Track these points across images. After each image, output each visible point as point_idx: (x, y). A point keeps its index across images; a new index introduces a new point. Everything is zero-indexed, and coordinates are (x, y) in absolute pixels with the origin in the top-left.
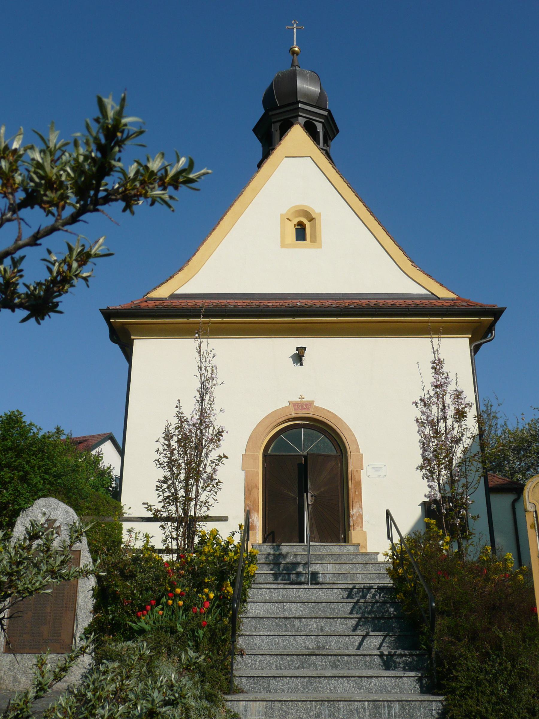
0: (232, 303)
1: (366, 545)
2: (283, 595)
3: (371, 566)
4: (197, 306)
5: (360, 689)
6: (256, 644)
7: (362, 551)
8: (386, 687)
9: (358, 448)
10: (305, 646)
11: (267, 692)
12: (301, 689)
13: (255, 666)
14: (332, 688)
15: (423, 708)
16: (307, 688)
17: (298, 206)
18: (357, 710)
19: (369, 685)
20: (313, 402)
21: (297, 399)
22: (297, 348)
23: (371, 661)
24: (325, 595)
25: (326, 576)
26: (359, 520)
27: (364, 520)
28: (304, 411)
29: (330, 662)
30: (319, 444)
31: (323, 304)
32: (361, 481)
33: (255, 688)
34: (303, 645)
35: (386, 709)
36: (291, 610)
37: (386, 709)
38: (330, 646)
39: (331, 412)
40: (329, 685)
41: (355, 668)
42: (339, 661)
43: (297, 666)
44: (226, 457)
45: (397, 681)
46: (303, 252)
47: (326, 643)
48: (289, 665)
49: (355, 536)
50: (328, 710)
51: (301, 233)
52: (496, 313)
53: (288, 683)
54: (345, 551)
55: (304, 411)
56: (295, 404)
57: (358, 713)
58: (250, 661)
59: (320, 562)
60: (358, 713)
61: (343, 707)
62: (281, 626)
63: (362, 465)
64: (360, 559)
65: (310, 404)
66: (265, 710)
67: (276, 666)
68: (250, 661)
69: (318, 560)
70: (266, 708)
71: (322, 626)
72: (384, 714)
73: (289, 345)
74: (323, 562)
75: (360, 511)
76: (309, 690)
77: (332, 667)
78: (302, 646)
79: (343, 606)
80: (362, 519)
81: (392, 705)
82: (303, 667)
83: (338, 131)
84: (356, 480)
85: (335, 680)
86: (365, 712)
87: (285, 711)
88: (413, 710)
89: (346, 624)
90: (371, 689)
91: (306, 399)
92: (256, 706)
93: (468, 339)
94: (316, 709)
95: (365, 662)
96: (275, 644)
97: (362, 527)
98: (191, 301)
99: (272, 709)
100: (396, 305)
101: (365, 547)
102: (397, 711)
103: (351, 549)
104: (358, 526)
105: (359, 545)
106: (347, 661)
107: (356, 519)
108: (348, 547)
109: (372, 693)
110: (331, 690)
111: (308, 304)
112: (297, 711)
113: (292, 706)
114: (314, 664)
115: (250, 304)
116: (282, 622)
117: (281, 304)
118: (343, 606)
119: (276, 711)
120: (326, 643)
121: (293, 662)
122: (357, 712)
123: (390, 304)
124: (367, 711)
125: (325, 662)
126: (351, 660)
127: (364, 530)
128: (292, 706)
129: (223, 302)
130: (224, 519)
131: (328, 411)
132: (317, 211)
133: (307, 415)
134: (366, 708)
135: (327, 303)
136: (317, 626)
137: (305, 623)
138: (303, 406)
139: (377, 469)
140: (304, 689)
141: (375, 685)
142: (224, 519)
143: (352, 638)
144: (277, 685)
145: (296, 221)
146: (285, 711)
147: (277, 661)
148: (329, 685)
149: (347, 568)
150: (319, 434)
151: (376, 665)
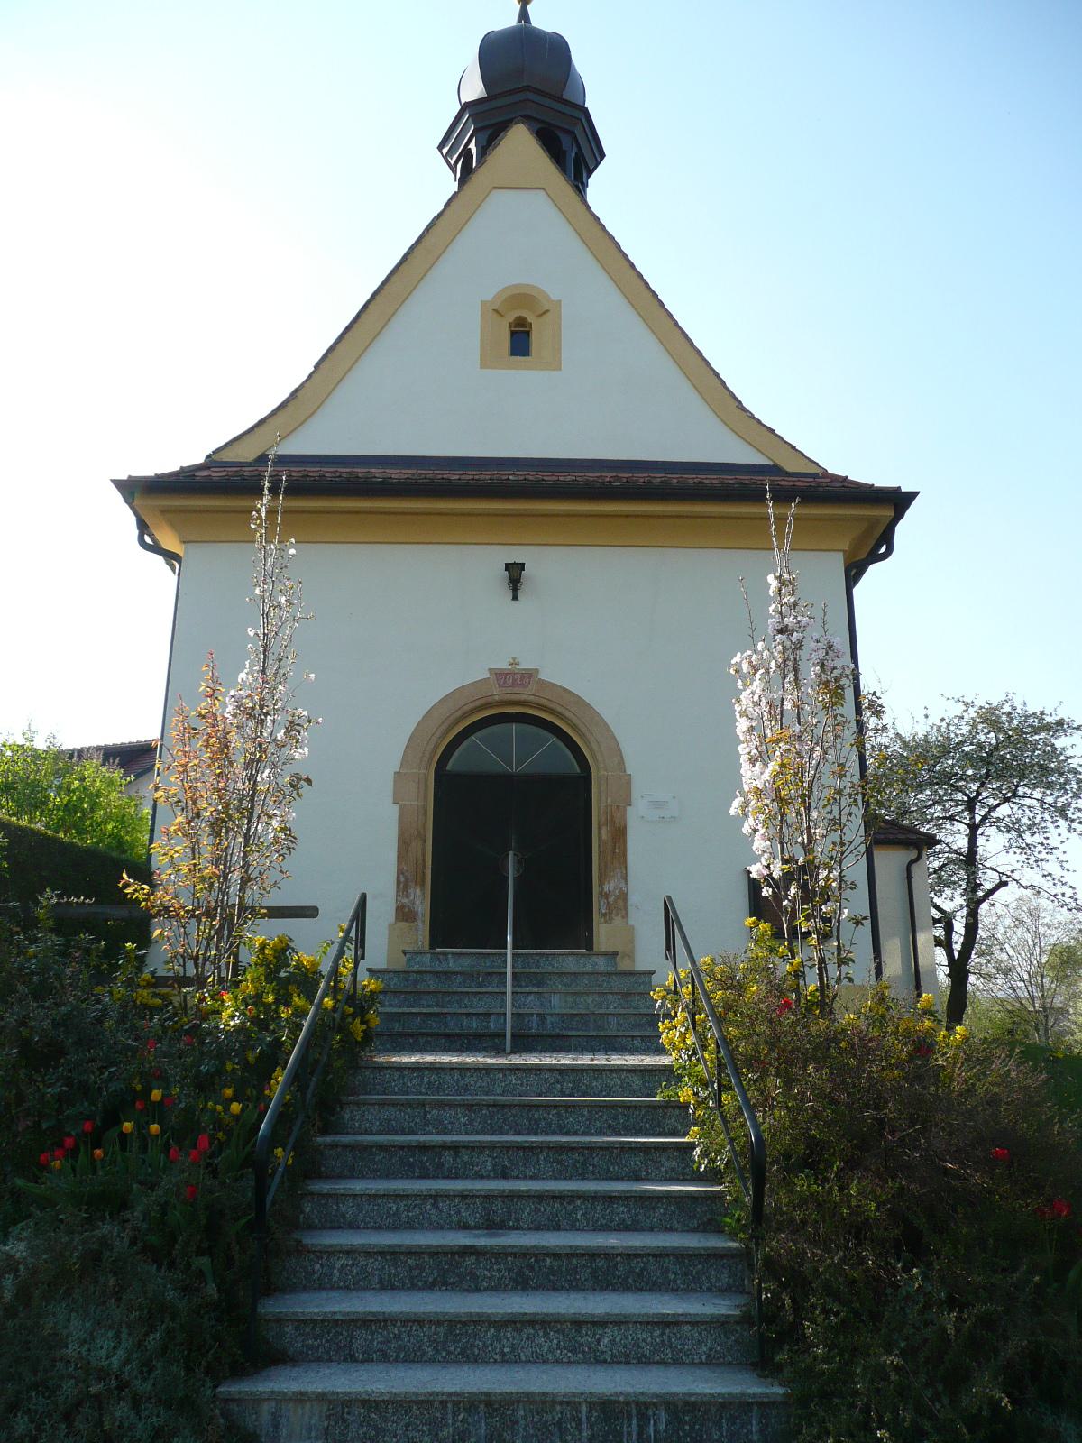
0: (377, 473)
1: (632, 951)
2: (429, 1083)
3: (637, 998)
4: (308, 479)
5: (575, 1352)
6: (344, 1216)
7: (624, 965)
8: (639, 1347)
9: (621, 761)
10: (459, 1222)
11: (345, 1360)
12: (430, 1352)
13: (330, 1280)
14: (506, 1350)
15: (727, 1420)
16: (444, 1349)
17: (516, 286)
18: (559, 1423)
19: (599, 1341)
20: (537, 670)
21: (504, 666)
22: (507, 565)
23: (609, 1267)
24: (522, 1085)
25: (545, 1019)
26: (620, 902)
27: (629, 902)
28: (516, 690)
29: (510, 1270)
30: (539, 756)
31: (561, 478)
32: (625, 827)
33: (317, 1348)
34: (455, 1218)
35: (634, 1422)
36: (441, 1123)
37: (634, 1422)
38: (518, 1220)
39: (570, 692)
40: (499, 1340)
41: (571, 1286)
42: (531, 1268)
43: (430, 1279)
44: (309, 781)
45: (667, 1331)
46: (522, 379)
47: (509, 1213)
48: (412, 1278)
49: (604, 934)
50: (487, 1424)
51: (520, 340)
52: (899, 501)
53: (398, 1337)
54: (589, 968)
55: (516, 690)
56: (499, 675)
57: (563, 1431)
58: (317, 1267)
59: (536, 990)
60: (563, 1431)
61: (525, 1418)
62: (411, 1166)
63: (629, 795)
64: (618, 984)
65: (529, 675)
66: (326, 1424)
67: (381, 1282)
68: (317, 1267)
69: (534, 985)
70: (328, 1418)
71: (504, 1167)
72: (629, 1434)
73: (490, 560)
74: (541, 990)
75: (623, 885)
76: (449, 1353)
77: (515, 1281)
78: (451, 1222)
79: (559, 1114)
80: (625, 900)
81: (650, 1413)
82: (445, 1283)
83: (603, 155)
84: (617, 825)
85: (515, 1330)
86: (580, 1431)
87: (376, 1428)
88: (702, 1425)
89: (561, 1162)
90: (603, 1352)
91: (525, 665)
92: (303, 1414)
93: (841, 554)
94: (454, 1422)
95: (594, 1273)
96: (389, 1215)
97: (625, 916)
98: (298, 469)
99: (344, 1420)
100: (703, 483)
101: (631, 956)
102: (662, 1427)
103: (602, 964)
104: (617, 915)
105: (615, 954)
106: (551, 1268)
107: (615, 901)
108: (595, 959)
109: (605, 1361)
110: (503, 1354)
111: (531, 478)
112: (407, 1425)
113: (394, 1414)
114: (472, 1274)
115: (416, 477)
116: (413, 1156)
117: (477, 477)
118: (559, 1114)
119: (354, 1427)
120: (509, 1213)
121: (422, 1269)
122: (560, 1428)
123: (691, 481)
124: (584, 1426)
125: (499, 1271)
126: (559, 1267)
127: (631, 922)
128: (394, 1414)
129: (360, 471)
130: (310, 912)
131: (565, 690)
132: (554, 296)
133: (523, 697)
134: (584, 1419)
135: (569, 478)
136: (494, 1166)
137: (466, 1158)
138: (514, 680)
139: (657, 805)
140: (437, 1351)
141: (613, 1342)
142: (310, 912)
143: (569, 1203)
144: (372, 1340)
145: (511, 317)
146: (376, 1428)
147: (383, 1268)
148: (499, 1340)
149: (590, 1001)
150: (508, 725)
151: (619, 1277)
